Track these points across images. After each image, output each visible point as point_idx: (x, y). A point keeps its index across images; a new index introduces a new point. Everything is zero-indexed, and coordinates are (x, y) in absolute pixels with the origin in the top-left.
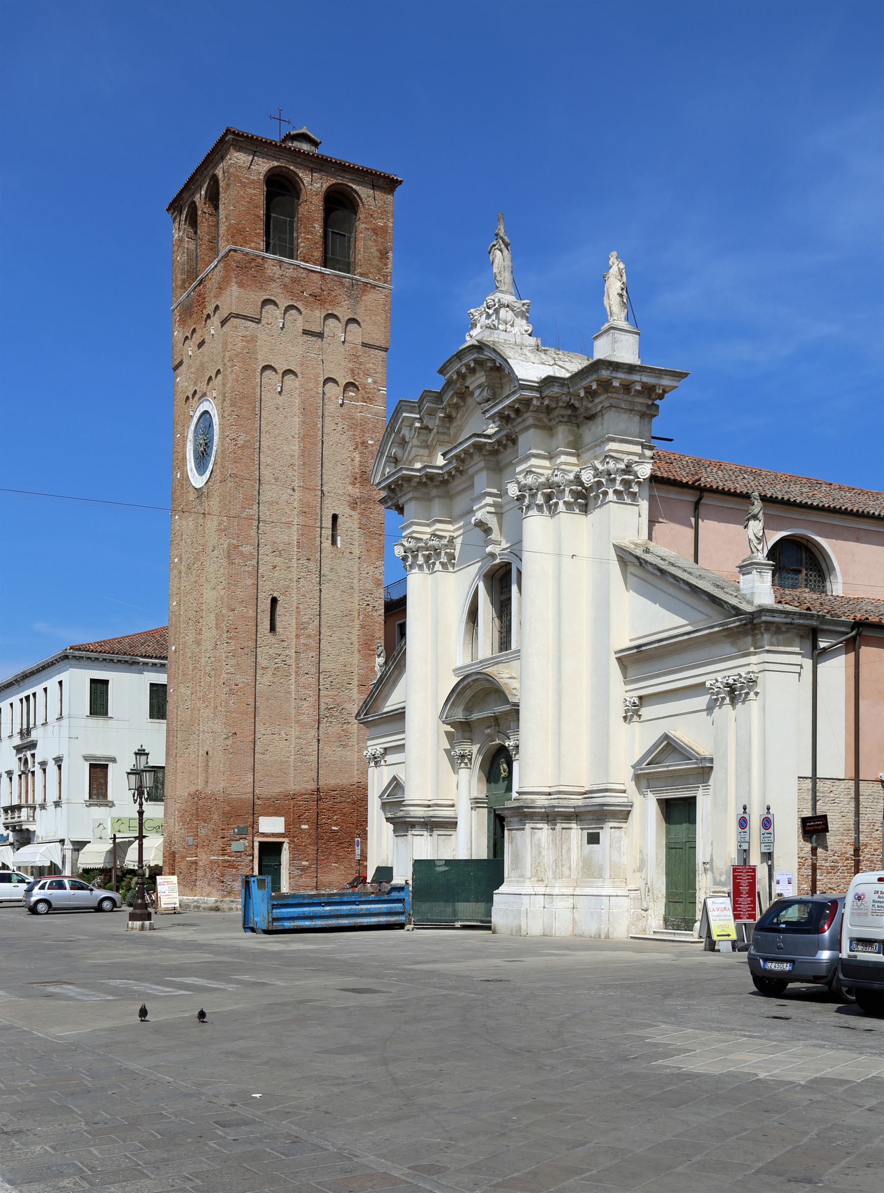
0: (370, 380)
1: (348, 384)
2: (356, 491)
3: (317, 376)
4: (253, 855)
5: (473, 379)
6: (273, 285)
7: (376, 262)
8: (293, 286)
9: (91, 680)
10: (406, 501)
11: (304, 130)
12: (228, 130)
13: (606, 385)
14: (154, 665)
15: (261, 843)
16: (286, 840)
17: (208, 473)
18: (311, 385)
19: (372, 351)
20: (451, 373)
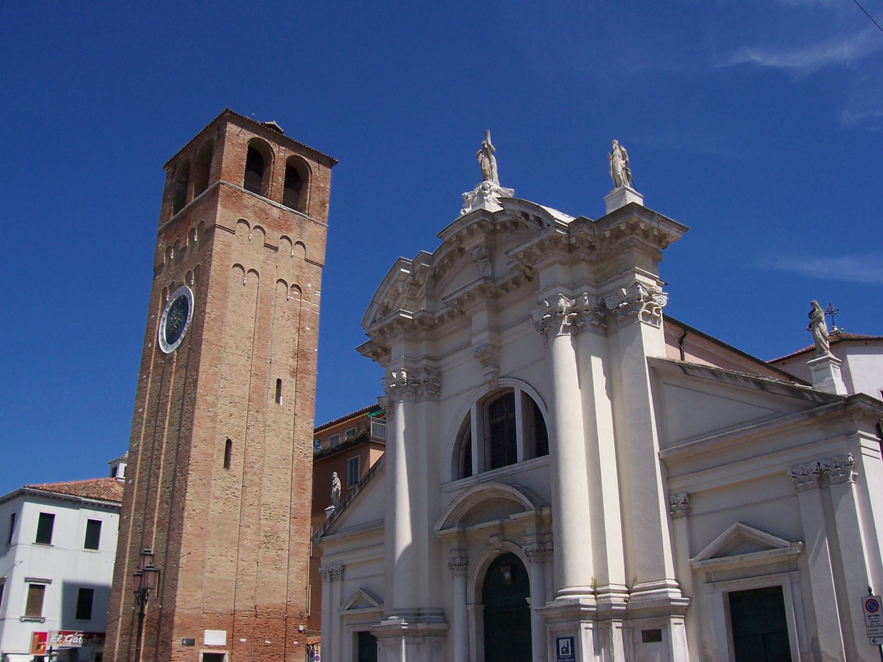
0: (309, 285)
1: (294, 286)
2: (293, 362)
3: (273, 276)
6: (247, 211)
7: (318, 208)
8: (262, 214)
9: (41, 514)
11: (274, 123)
12: (227, 110)
14: (93, 504)
16: (227, 652)
17: (179, 341)
18: (267, 282)
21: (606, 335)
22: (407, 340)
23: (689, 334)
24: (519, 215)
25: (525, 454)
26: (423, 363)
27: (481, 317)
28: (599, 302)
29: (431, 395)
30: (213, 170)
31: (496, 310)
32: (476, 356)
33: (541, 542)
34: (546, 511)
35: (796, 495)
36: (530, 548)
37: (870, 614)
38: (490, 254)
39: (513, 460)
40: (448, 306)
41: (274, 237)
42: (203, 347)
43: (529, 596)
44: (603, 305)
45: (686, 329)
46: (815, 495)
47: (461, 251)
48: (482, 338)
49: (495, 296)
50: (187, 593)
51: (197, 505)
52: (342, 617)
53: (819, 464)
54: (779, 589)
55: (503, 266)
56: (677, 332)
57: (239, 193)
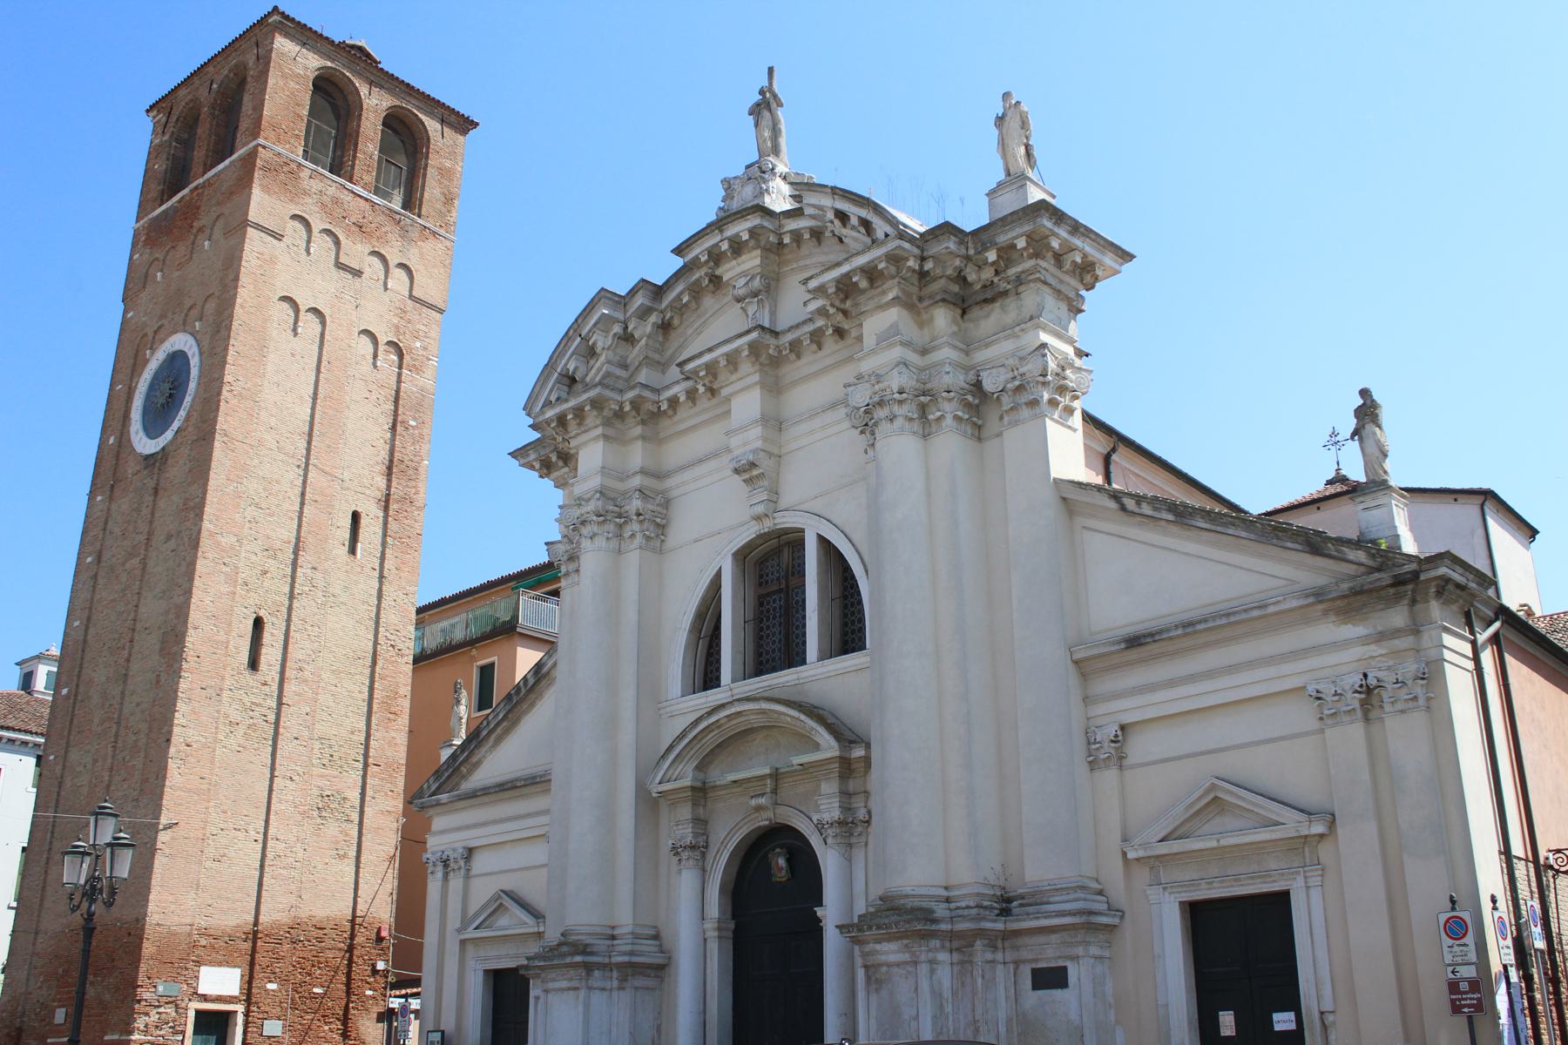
0: (418, 344)
1: (390, 343)
4: (183, 1033)
5: (734, 262)
6: (309, 200)
7: (439, 206)
8: (330, 207)
10: (585, 444)
12: (276, 8)
13: (1038, 245)
15: (198, 1013)
17: (169, 435)
19: (425, 310)
20: (698, 250)
21: (979, 439)
22: (606, 437)
23: (1122, 449)
24: (830, 215)
25: (820, 650)
26: (637, 481)
27: (747, 403)
28: (971, 377)
29: (648, 538)
30: (244, 124)
31: (774, 388)
32: (737, 471)
33: (847, 808)
34: (859, 752)
35: (1322, 731)
36: (826, 817)
37: (1451, 942)
38: (768, 288)
39: (794, 657)
40: (688, 378)
41: (356, 251)
42: (217, 444)
43: (820, 904)
44: (978, 385)
45: (1121, 440)
46: (1355, 731)
47: (716, 281)
48: (749, 441)
49: (776, 362)
50: (171, 898)
51: (192, 735)
52: (463, 942)
53: (1365, 676)
54: (1284, 897)
55: (795, 304)
56: (1102, 444)
57: (293, 166)
